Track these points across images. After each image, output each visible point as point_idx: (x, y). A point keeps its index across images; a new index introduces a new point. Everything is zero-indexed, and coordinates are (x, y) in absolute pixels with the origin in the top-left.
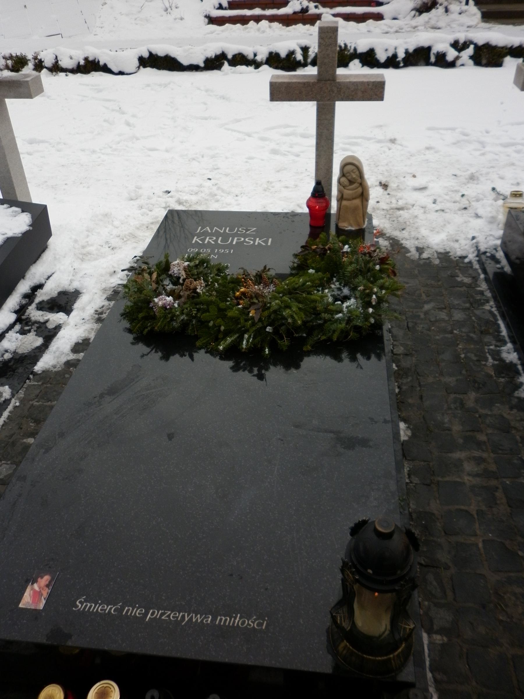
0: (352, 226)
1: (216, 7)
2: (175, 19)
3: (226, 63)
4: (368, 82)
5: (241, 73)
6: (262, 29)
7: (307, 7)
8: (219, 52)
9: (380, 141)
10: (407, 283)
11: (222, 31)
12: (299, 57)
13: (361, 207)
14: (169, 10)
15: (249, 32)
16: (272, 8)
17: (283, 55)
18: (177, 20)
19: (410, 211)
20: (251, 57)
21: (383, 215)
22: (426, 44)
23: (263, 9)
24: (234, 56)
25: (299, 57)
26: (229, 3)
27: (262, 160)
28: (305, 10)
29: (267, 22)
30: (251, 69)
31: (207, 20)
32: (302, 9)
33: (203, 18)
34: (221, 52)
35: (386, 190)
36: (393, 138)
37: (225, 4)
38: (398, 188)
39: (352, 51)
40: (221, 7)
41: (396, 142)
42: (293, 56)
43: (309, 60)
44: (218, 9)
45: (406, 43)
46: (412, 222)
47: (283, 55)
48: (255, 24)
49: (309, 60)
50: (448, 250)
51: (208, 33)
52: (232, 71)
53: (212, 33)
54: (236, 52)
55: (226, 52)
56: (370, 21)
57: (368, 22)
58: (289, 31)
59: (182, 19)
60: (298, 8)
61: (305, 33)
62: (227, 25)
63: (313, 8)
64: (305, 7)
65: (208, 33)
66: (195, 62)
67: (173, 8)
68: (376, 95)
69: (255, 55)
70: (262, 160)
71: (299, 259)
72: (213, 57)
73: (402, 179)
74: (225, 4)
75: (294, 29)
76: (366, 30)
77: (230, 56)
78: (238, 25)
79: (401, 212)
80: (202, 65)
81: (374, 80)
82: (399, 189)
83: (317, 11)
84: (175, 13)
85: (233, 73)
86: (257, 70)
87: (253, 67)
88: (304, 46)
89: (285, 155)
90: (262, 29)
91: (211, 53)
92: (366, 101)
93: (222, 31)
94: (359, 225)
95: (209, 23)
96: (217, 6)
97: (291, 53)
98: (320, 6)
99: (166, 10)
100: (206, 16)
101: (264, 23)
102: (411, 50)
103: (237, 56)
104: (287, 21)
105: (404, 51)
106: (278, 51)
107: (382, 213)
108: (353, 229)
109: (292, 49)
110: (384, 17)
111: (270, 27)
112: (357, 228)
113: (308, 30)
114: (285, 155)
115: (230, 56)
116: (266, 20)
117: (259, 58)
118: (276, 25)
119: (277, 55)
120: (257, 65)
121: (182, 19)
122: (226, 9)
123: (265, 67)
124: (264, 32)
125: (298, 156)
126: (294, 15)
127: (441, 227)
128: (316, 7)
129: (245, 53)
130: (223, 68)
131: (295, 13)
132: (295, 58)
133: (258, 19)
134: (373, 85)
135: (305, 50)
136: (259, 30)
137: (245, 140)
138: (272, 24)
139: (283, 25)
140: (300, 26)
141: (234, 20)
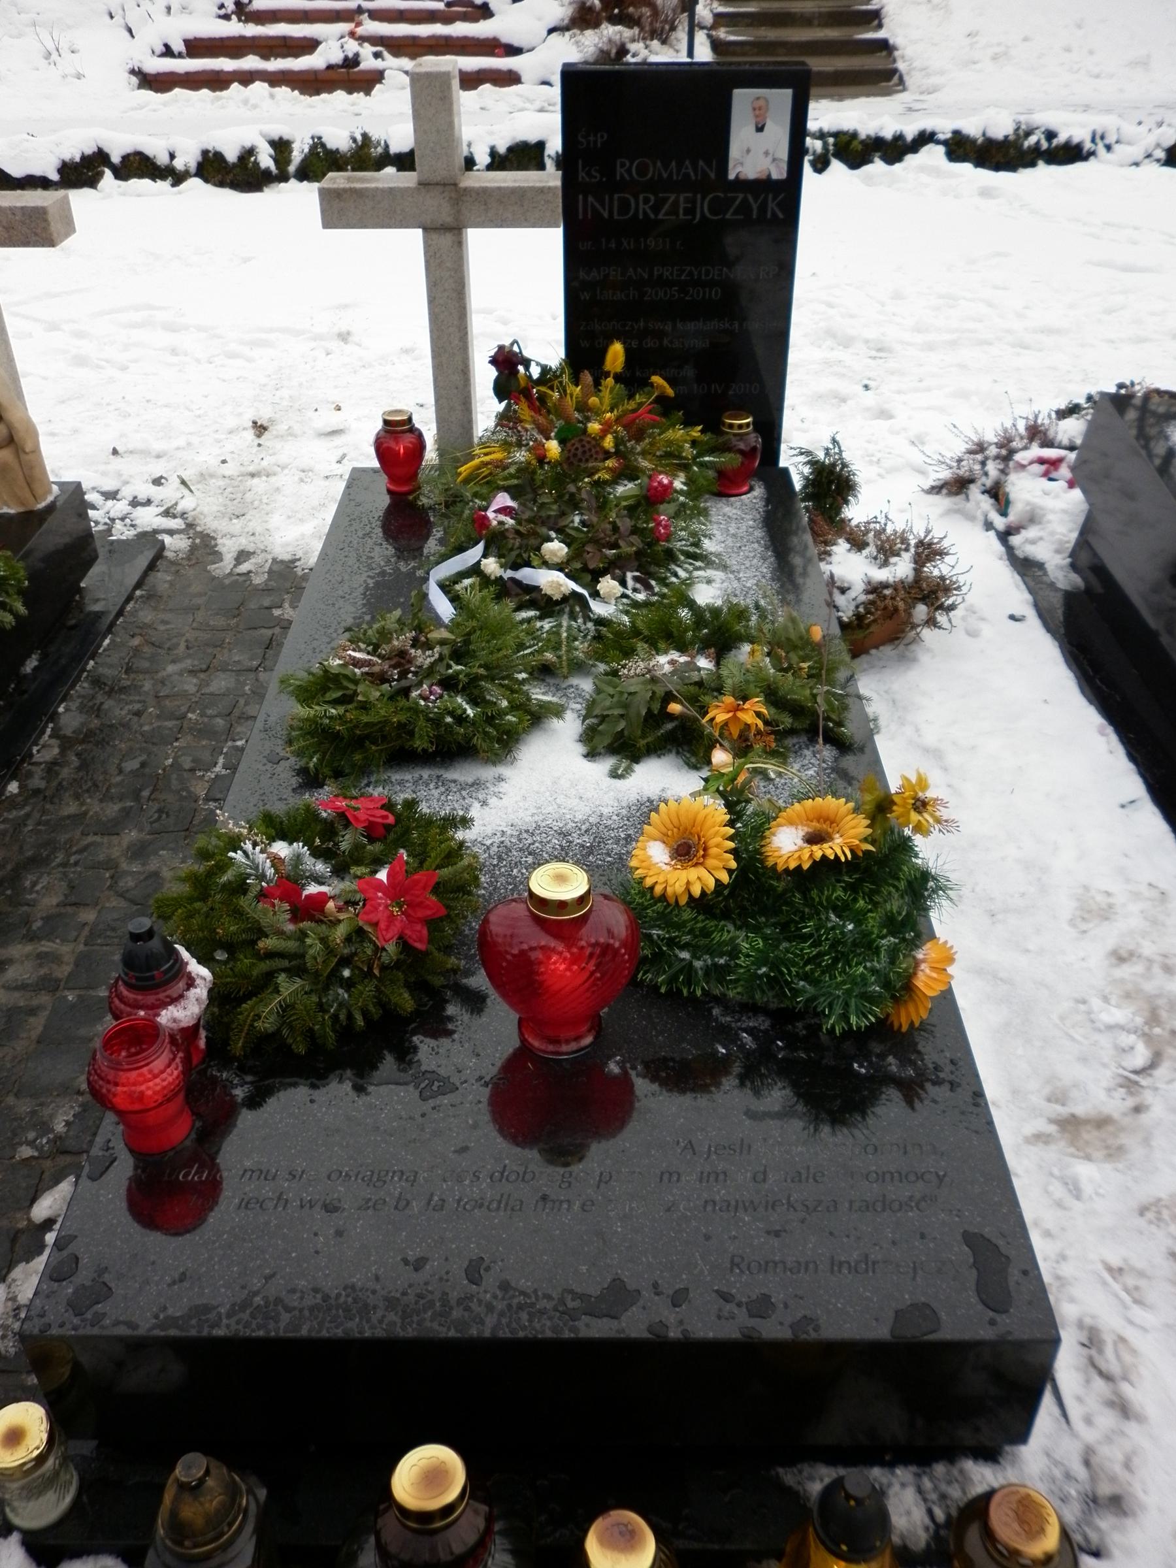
0: (9, 506)
1: (158, 52)
2: (65, 76)
3: (108, 173)
4: (10, 208)
5: (139, 196)
6: (252, 101)
7: (357, 55)
8: (89, 150)
9: (317, 338)
10: (167, 623)
11: (165, 104)
12: (266, 160)
13: (16, 465)
14: (55, 55)
15: (223, 107)
16: (284, 56)
17: (231, 156)
18: (70, 79)
19: (273, 479)
20: (162, 159)
21: (220, 487)
22: (532, 137)
23: (265, 57)
24: (126, 158)
25: (266, 160)
26: (187, 42)
27: (45, 378)
28: (351, 62)
29: (266, 85)
30: (164, 186)
31: (135, 80)
32: (346, 59)
33: (127, 75)
34: (96, 150)
35: (259, 436)
36: (344, 329)
37: (178, 46)
38: (291, 434)
39: (380, 150)
40: (168, 52)
41: (350, 339)
42: (252, 159)
43: (292, 169)
44: (163, 55)
45: (491, 133)
46: (265, 501)
47: (231, 156)
48: (241, 87)
49: (292, 169)
50: (299, 554)
51: (133, 109)
52: (120, 190)
53: (141, 108)
54: (129, 149)
55: (106, 150)
56: (487, 88)
57: (481, 87)
58: (311, 107)
59: (79, 76)
60: (336, 57)
61: (344, 111)
62: (177, 91)
63: (371, 56)
64: (350, 55)
65: (133, 109)
66: (37, 171)
67: (65, 53)
68: (36, 234)
69: (172, 156)
70: (45, 378)
71: (786, 628)
72: (78, 159)
73: (311, 413)
74: (178, 46)
75: (324, 101)
76: (478, 107)
77: (116, 159)
78: (205, 92)
79: (256, 480)
80: (55, 177)
81: (23, 204)
82: (291, 435)
83: (378, 64)
84: (68, 63)
85: (124, 194)
86: (176, 189)
87: (169, 180)
88: (276, 138)
89: (99, 367)
90: (252, 101)
91: (73, 151)
92: (19, 246)
93: (165, 104)
94: (23, 504)
95: (140, 87)
96: (160, 49)
97: (249, 153)
98: (386, 54)
99: (48, 55)
100: (133, 72)
101: (259, 87)
102: (502, 149)
103: (131, 158)
104: (312, 84)
105: (488, 150)
106: (218, 149)
107: (221, 483)
108: (12, 511)
109: (248, 145)
110: (523, 80)
111: (272, 96)
112: (21, 510)
113: (353, 105)
114: (99, 367)
115: (116, 159)
116: (263, 80)
117: (179, 164)
118: (284, 91)
119: (219, 156)
120: (178, 178)
121: (79, 76)
122: (180, 56)
123: (195, 183)
124: (255, 107)
125: (124, 368)
126: (330, 72)
127: (313, 508)
128: (377, 55)
129: (149, 152)
130: (101, 185)
131: (330, 67)
132: (256, 163)
133: (246, 78)
134: (24, 214)
135: (281, 147)
136: (246, 102)
137: (30, 335)
138: (277, 89)
139: (302, 93)
140: (340, 95)
141: (192, 81)
